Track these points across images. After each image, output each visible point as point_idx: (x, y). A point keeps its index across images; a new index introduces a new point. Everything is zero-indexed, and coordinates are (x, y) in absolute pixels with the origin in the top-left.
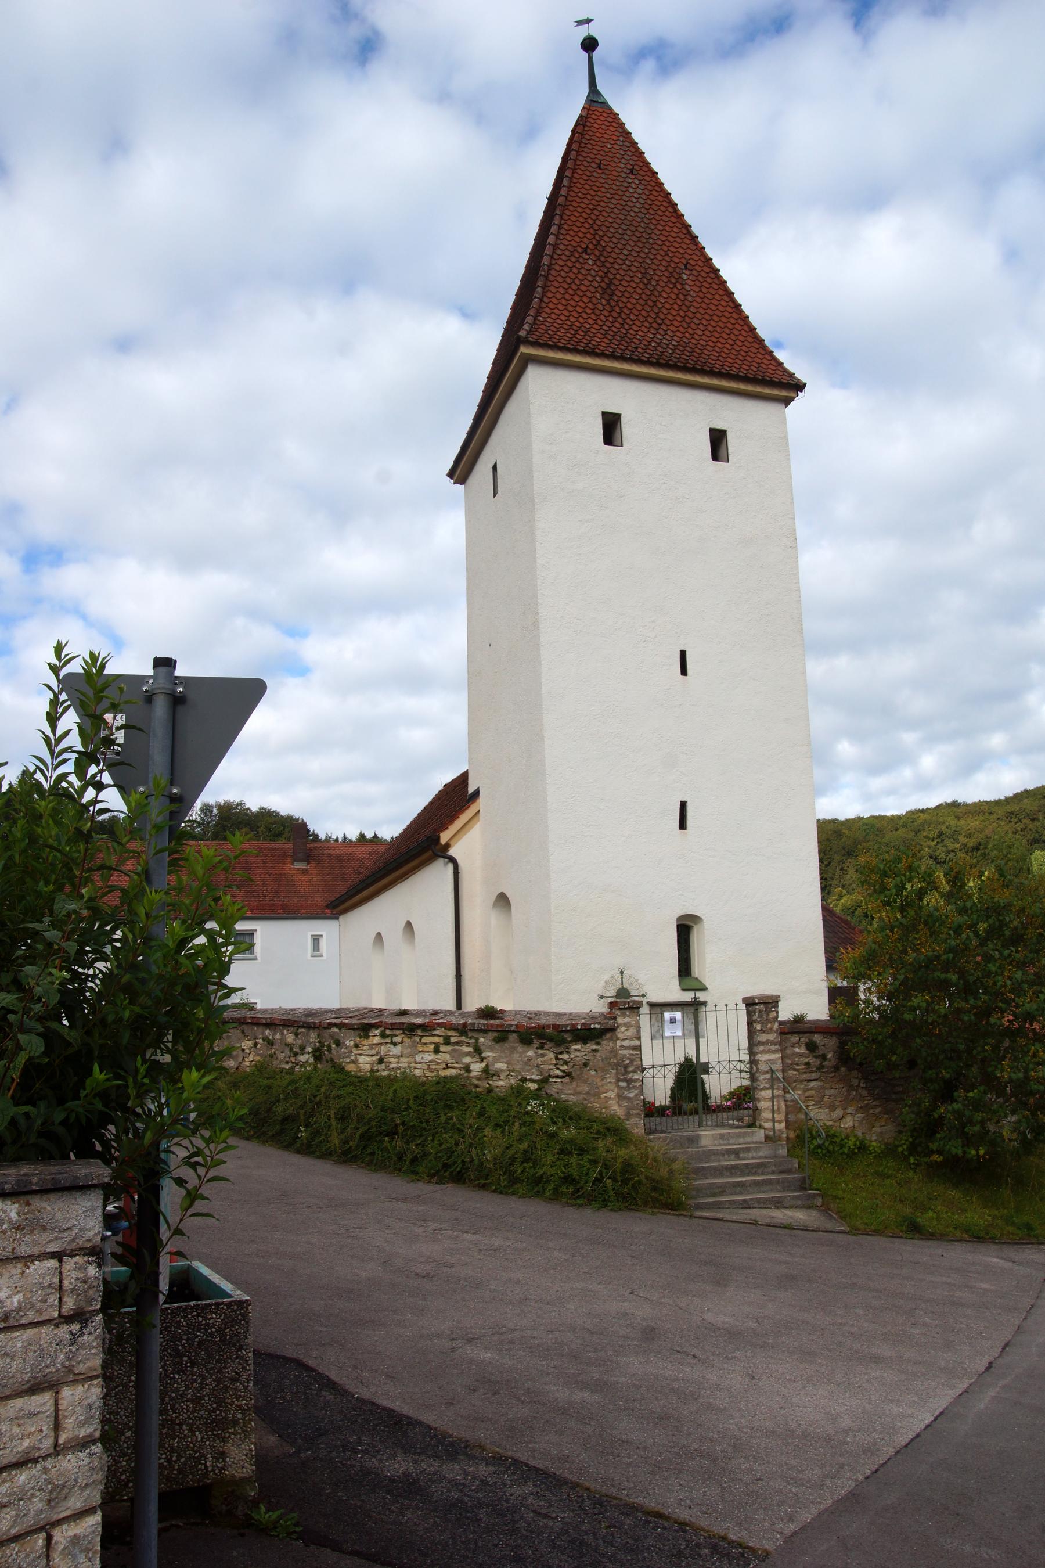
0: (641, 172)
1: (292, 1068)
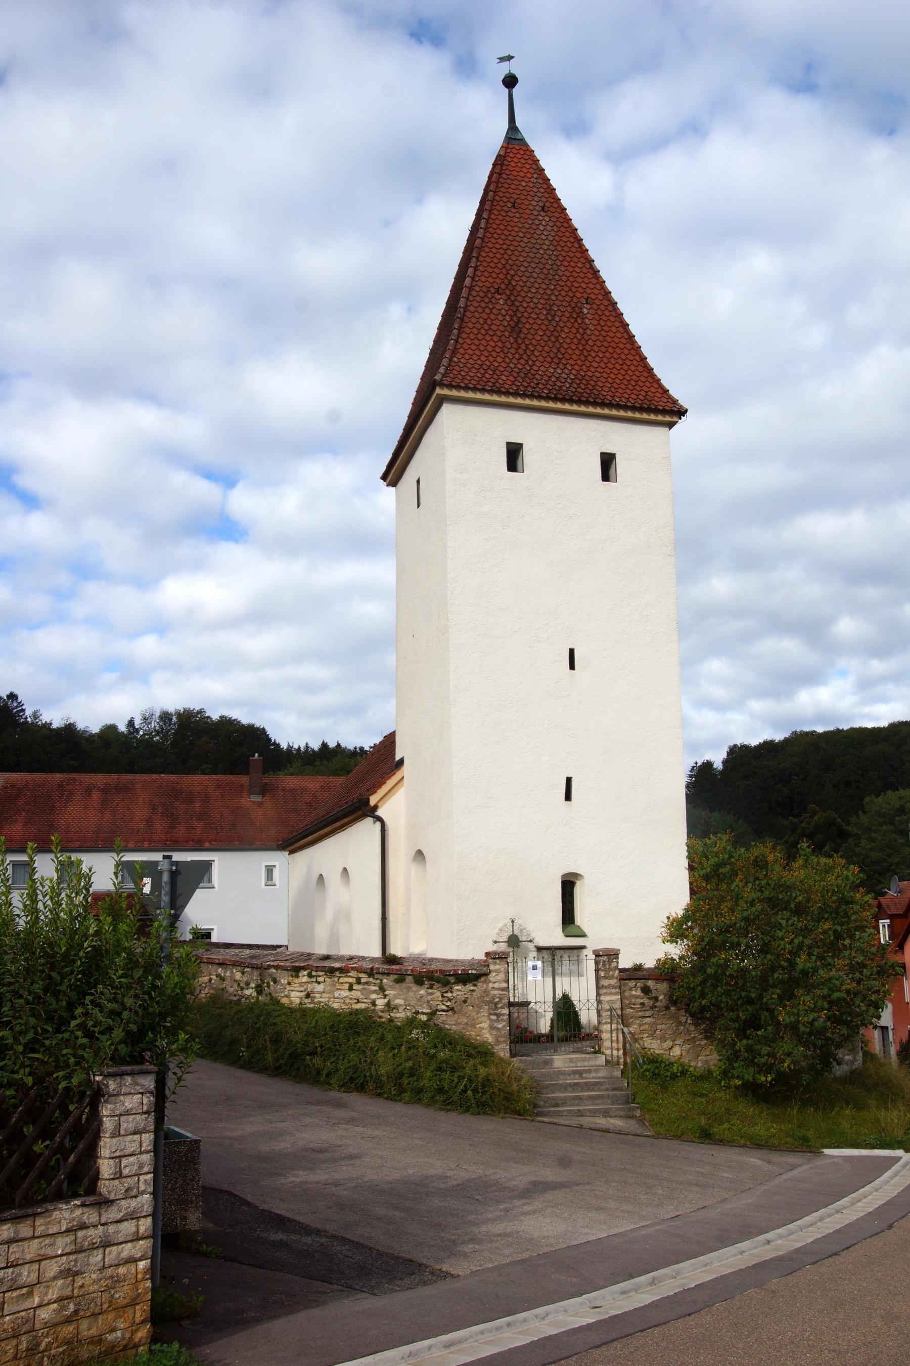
0: (552, 209)
1: (239, 1000)
